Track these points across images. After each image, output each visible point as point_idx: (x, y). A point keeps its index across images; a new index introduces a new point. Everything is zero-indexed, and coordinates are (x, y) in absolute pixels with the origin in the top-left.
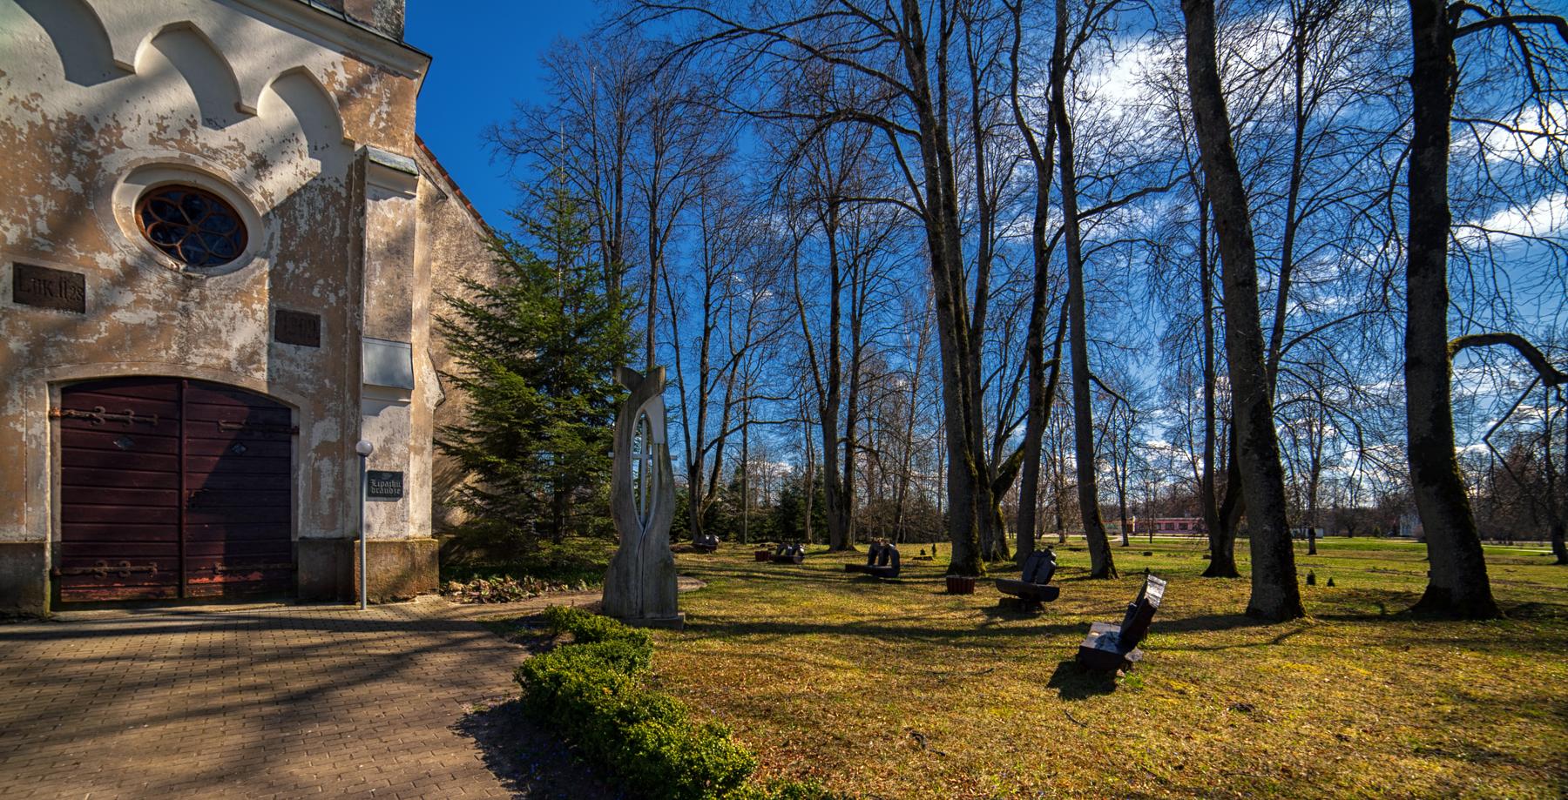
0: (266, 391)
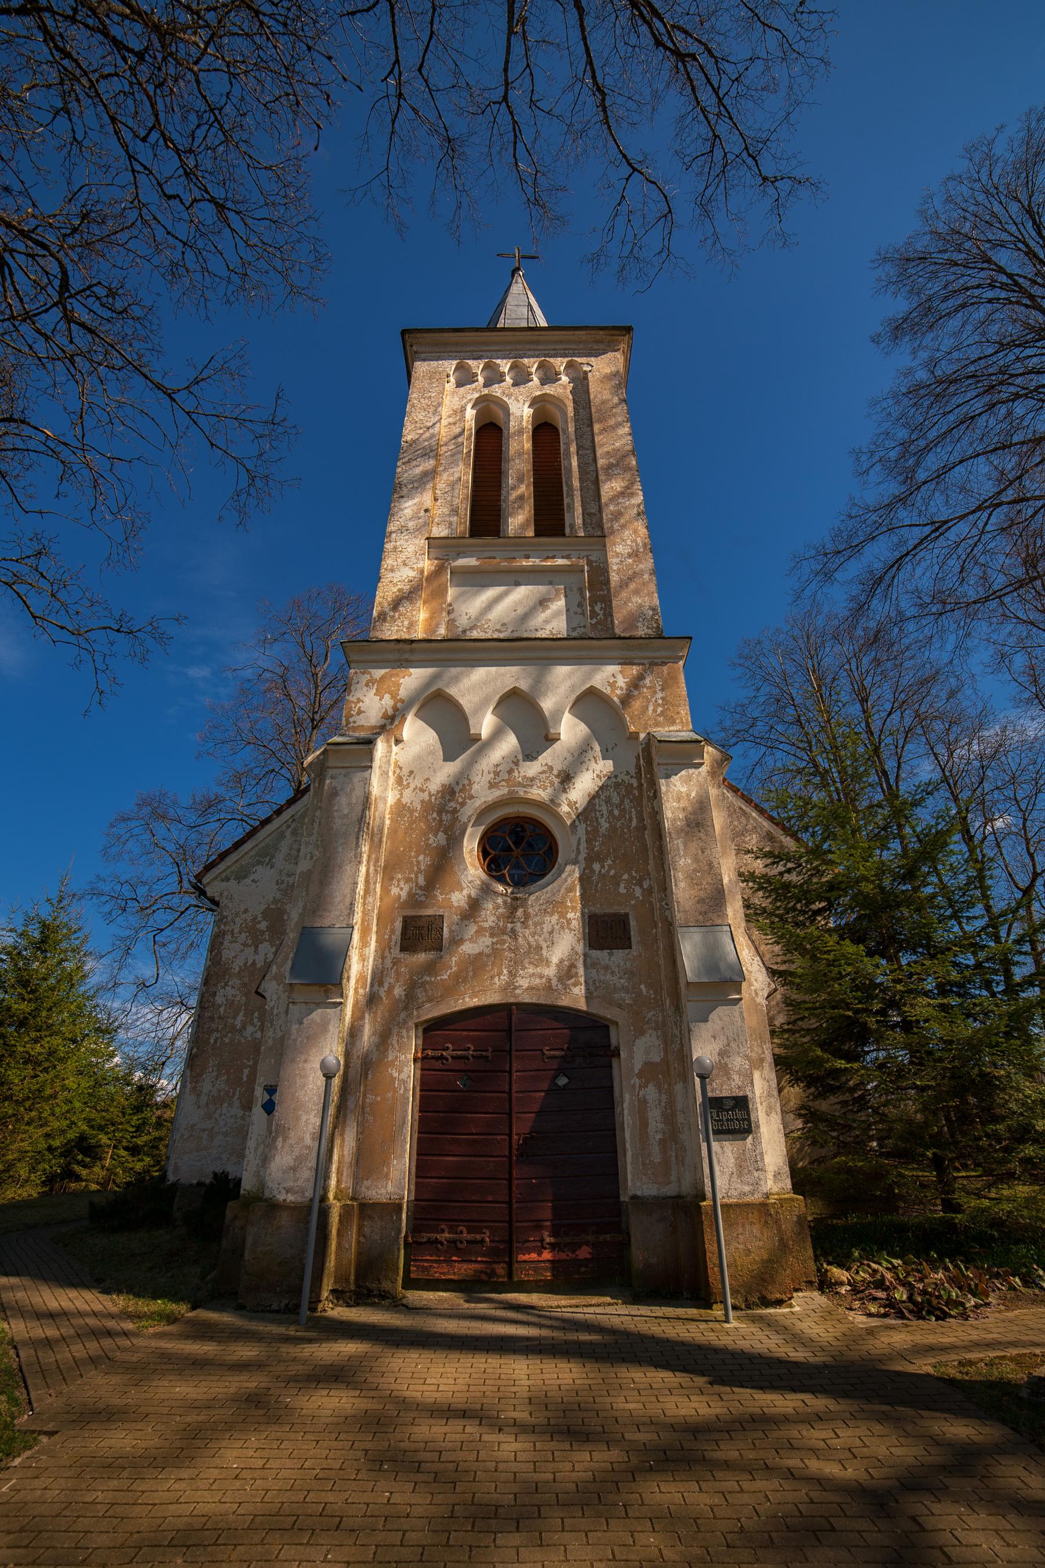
0: (584, 1008)
